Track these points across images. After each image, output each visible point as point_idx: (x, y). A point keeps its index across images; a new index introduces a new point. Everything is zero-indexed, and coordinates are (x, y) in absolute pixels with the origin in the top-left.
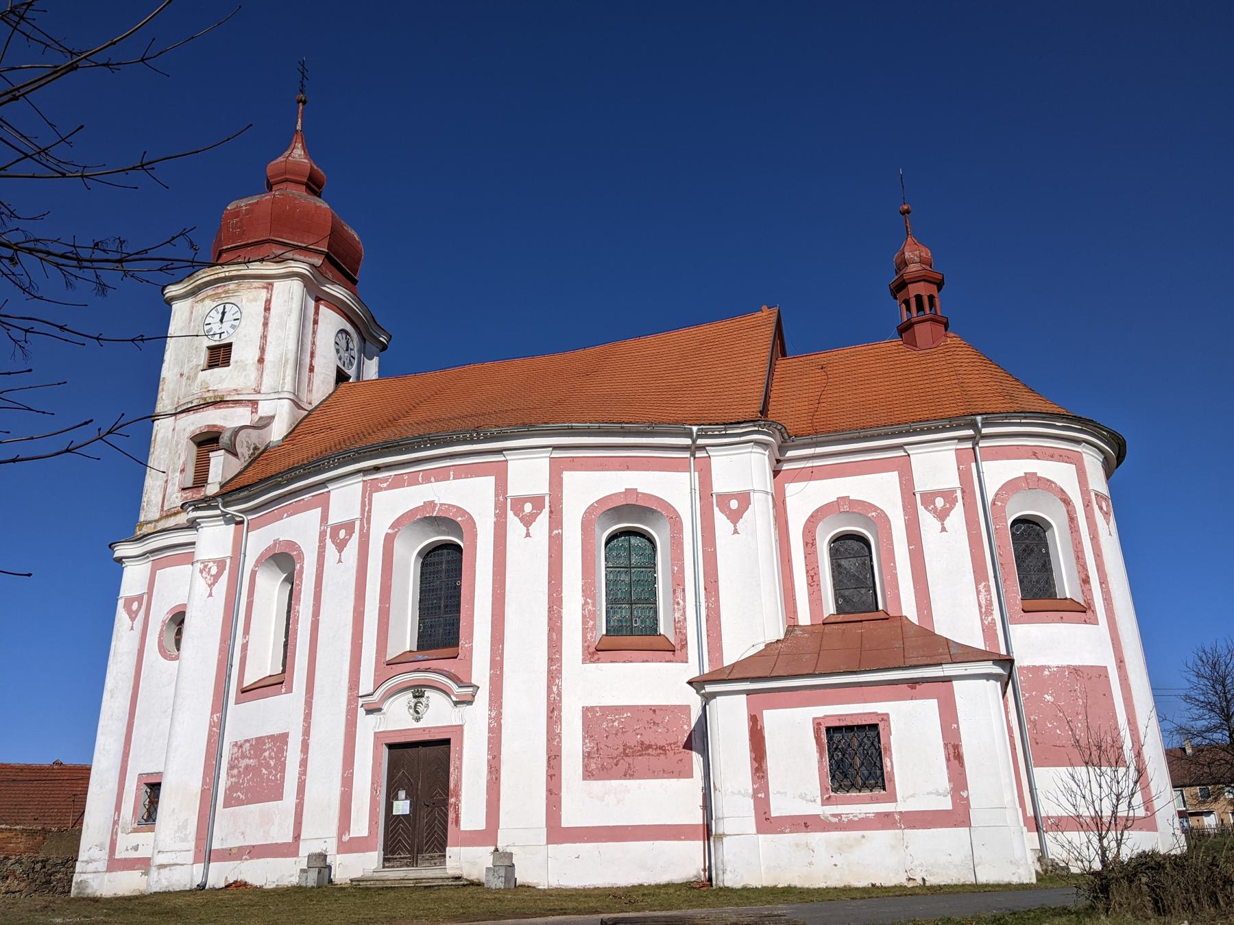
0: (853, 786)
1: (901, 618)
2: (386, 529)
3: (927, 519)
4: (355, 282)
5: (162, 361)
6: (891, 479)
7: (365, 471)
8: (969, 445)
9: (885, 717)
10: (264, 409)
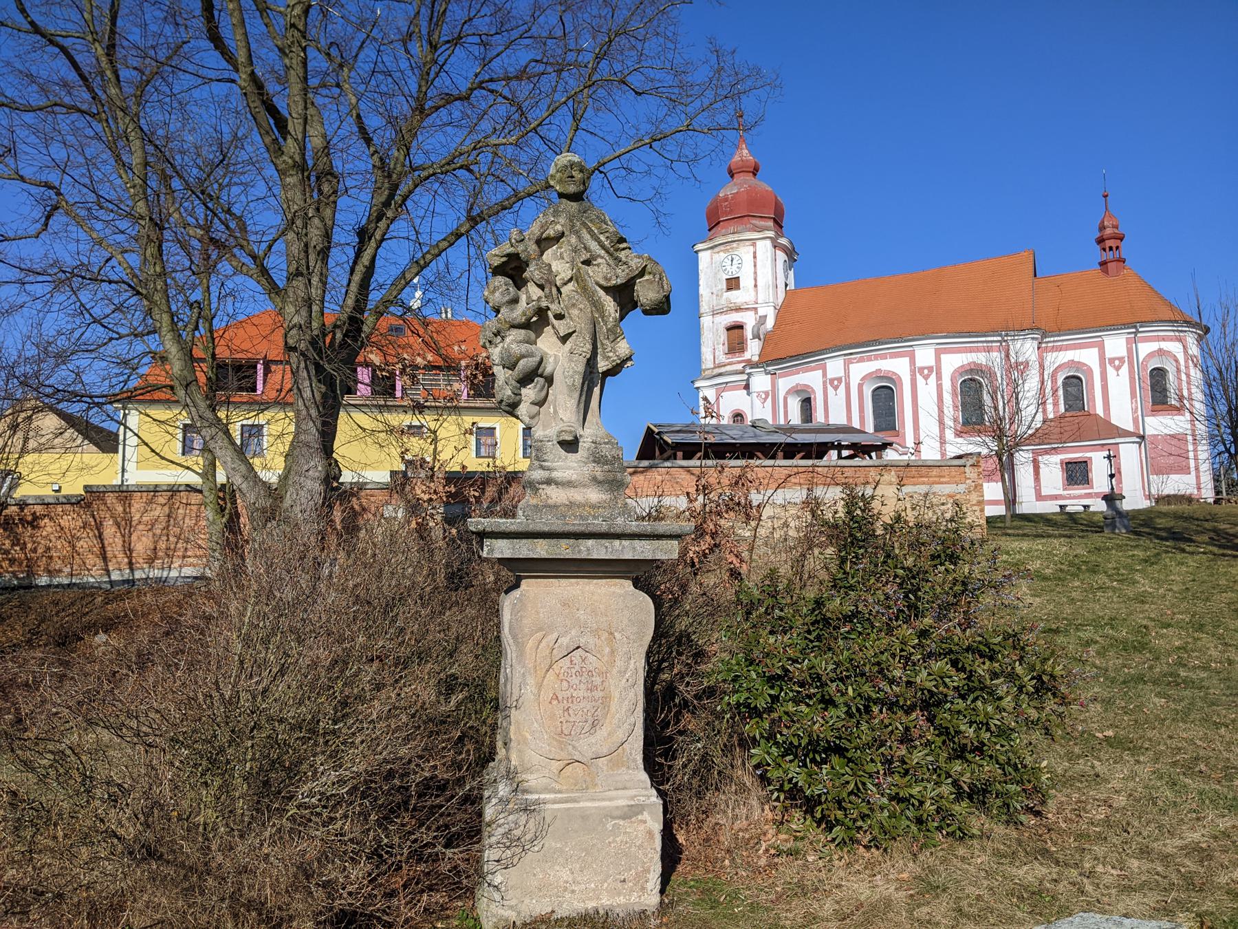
0: (1076, 483)
2: (858, 381)
3: (1110, 371)
4: (781, 227)
5: (698, 285)
6: (1094, 352)
7: (845, 355)
9: (1090, 458)
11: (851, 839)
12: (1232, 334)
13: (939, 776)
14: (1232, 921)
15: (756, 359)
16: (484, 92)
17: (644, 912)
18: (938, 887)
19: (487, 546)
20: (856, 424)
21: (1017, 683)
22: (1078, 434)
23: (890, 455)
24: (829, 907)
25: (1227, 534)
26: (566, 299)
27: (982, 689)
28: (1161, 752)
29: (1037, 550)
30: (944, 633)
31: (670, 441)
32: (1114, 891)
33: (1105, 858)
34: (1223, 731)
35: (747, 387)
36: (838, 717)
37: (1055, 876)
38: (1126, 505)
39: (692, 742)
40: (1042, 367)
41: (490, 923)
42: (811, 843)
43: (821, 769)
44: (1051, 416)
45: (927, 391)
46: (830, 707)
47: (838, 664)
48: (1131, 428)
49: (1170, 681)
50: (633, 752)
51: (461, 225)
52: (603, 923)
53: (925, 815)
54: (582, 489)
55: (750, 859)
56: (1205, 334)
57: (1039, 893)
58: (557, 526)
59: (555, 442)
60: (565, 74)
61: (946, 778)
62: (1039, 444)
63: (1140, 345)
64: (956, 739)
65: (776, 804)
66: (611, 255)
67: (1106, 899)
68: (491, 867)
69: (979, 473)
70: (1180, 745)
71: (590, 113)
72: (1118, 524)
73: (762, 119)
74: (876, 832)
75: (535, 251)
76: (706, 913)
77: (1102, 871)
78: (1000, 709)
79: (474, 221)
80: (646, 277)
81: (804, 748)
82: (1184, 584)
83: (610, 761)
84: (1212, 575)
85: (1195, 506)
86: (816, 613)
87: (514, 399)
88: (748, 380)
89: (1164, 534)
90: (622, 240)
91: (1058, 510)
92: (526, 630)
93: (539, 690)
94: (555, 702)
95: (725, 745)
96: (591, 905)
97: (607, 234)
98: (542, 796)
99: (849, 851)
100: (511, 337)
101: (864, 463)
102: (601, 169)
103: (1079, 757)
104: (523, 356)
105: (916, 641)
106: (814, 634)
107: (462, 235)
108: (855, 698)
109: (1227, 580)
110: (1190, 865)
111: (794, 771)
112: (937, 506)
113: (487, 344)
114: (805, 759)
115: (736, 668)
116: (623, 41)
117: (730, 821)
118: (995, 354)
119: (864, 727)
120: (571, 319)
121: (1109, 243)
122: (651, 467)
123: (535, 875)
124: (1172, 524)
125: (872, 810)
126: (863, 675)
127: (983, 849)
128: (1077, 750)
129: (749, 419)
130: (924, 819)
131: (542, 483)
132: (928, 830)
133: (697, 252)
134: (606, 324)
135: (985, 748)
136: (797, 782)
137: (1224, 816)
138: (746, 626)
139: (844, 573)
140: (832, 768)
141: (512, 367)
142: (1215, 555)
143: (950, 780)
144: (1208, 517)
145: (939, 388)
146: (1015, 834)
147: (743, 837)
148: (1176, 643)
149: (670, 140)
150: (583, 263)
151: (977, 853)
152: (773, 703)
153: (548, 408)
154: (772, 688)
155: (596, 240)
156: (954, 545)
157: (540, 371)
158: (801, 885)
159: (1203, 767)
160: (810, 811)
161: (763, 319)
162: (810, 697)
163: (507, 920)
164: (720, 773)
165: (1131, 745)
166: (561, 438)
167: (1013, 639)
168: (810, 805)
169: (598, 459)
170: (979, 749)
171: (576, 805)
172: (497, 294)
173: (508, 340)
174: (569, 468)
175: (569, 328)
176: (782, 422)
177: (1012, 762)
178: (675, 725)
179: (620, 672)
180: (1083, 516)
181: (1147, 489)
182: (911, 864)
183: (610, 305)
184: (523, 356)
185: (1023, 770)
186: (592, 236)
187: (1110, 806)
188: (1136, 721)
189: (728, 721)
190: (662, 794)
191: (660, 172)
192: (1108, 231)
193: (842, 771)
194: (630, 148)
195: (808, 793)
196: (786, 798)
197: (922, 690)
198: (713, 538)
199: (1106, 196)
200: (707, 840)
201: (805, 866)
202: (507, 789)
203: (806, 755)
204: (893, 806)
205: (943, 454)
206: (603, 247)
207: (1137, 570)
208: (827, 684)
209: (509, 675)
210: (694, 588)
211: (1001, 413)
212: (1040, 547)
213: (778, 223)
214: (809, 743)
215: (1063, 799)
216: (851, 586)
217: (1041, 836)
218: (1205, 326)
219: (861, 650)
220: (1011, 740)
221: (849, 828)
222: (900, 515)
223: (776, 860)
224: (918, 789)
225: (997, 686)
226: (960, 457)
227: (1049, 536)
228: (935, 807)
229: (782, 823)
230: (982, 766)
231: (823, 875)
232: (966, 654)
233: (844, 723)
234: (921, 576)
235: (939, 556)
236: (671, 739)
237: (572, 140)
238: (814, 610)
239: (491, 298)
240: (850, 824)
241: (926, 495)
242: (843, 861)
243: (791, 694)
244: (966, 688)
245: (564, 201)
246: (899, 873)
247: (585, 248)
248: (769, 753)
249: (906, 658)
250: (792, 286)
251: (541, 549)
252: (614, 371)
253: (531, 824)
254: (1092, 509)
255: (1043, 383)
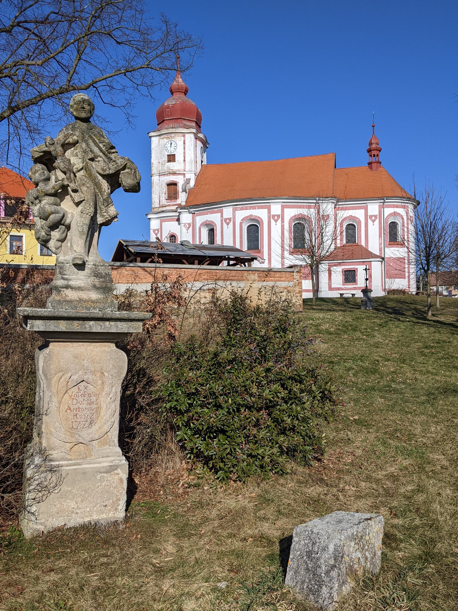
0: (349, 282)
1: (361, 246)
2: (240, 221)
3: (370, 222)
5: (151, 157)
7: (234, 205)
8: (382, 204)
9: (357, 269)
10: (187, 176)
11: (227, 477)
12: (430, 207)
13: (272, 443)
14: (404, 510)
15: (184, 204)
16: (21, 29)
17: (116, 521)
18: (269, 500)
19: (30, 324)
20: (238, 246)
21: (313, 395)
22: (351, 256)
23: (255, 264)
24: (214, 512)
25: (421, 311)
26: (79, 180)
27: (295, 398)
28: (380, 427)
29: (327, 318)
30: (278, 370)
31: (133, 251)
32: (352, 498)
33: (350, 482)
34: (409, 416)
35: (178, 220)
36: (223, 414)
37: (326, 492)
38: (373, 295)
39: (145, 428)
40: (336, 219)
41: (29, 533)
42: (206, 480)
43: (213, 441)
44: (339, 246)
45: (276, 228)
46: (219, 409)
47: (224, 387)
48: (378, 253)
49: (388, 389)
50: (113, 437)
51: (4, 112)
52: (94, 529)
53: (265, 464)
54: (87, 292)
55: (174, 490)
56: (418, 205)
57: (318, 501)
58: (71, 312)
59: (71, 264)
60: (73, 25)
61: (276, 444)
62: (332, 260)
63: (385, 209)
64: (282, 425)
65: (189, 460)
66: (106, 156)
67: (349, 503)
68: (30, 503)
69: (301, 276)
70: (389, 423)
71: (88, 50)
72: (368, 305)
73: (191, 66)
74: (240, 473)
75: (61, 151)
76: (149, 520)
77: (348, 488)
78: (303, 409)
79: (13, 109)
80: (127, 170)
81: (205, 431)
82: (398, 338)
83: (100, 442)
84: (411, 333)
85: (406, 296)
86: (214, 360)
87: (46, 237)
88: (179, 216)
89: (390, 310)
90: (113, 148)
91: (339, 296)
92: (53, 372)
93: (60, 404)
94: (69, 411)
95: (162, 429)
96: (87, 520)
97: (104, 144)
98: (61, 463)
99: (226, 484)
100: (45, 201)
101: (241, 269)
102: (94, 85)
103: (341, 430)
104: (52, 213)
105: (264, 374)
106: (213, 371)
107: (5, 118)
108: (232, 404)
109: (419, 336)
110: (389, 484)
111: (200, 443)
112: (278, 293)
113: (30, 204)
114: (205, 436)
115: (170, 389)
116: (110, 9)
117: (164, 470)
118: (312, 210)
119: (236, 419)
120: (82, 192)
121: (373, 152)
122: (121, 266)
123: (55, 506)
124: (394, 305)
125: (238, 462)
126: (237, 392)
127: (292, 480)
128: (340, 426)
129: (179, 240)
130: (264, 466)
131: (63, 288)
132: (266, 471)
133: (150, 137)
134: (102, 196)
135: (295, 428)
136: (200, 449)
137: (406, 459)
138: (177, 366)
139: (230, 338)
140: (219, 441)
141: (46, 219)
142: (414, 322)
143: (277, 445)
144: (413, 302)
145: (283, 227)
146: (307, 471)
147: (171, 478)
148: (392, 370)
149: (136, 72)
150: (90, 159)
151: (289, 481)
152: (189, 407)
153: (67, 244)
154: (189, 399)
155: (97, 147)
156: (285, 323)
157: (63, 222)
158: (200, 503)
159: (399, 435)
160: (206, 463)
161: (188, 181)
162: (209, 404)
163: (38, 530)
164: (159, 444)
165: (366, 424)
166: (75, 262)
167: (312, 373)
168: (207, 460)
169: (97, 275)
170: (293, 429)
171: (80, 467)
172: (37, 175)
173: (43, 202)
174: (79, 279)
175: (81, 198)
176: (198, 243)
177: (308, 435)
178: (135, 420)
179: (106, 394)
180: (351, 299)
181: (384, 286)
182: (256, 489)
183: (105, 185)
184: (52, 213)
185: (313, 439)
186: (95, 144)
187: (354, 455)
188: (369, 411)
189: (164, 416)
190: (128, 458)
191: (130, 90)
192: (374, 146)
193: (224, 443)
194: (112, 74)
195: (206, 454)
196: (194, 457)
197: (266, 399)
198: (160, 317)
199: (373, 126)
200: (151, 481)
201: (203, 492)
202: (40, 460)
203: (206, 435)
204: (249, 460)
205: (283, 265)
206: (101, 151)
207: (376, 330)
208: (218, 397)
209: (42, 396)
210: (149, 344)
211: (314, 243)
212: (329, 316)
213: (198, 125)
214: (208, 428)
215: (332, 452)
216: (233, 344)
217: (320, 472)
218: (417, 201)
219: (236, 378)
220: (309, 423)
221: (226, 472)
222: (259, 307)
223: (188, 490)
224: (262, 450)
225: (303, 397)
226: (291, 267)
227: (334, 311)
228: (270, 459)
229: (191, 470)
230: (293, 437)
231: (212, 497)
232: (288, 381)
233: (226, 417)
234: (268, 341)
235: (277, 328)
236: (134, 428)
237: (76, 65)
238: (213, 358)
239: (33, 177)
240: (227, 470)
241: (273, 287)
242: (222, 488)
243: (199, 402)
244: (288, 398)
245: (78, 121)
246: (251, 493)
247: (91, 151)
248: (186, 434)
249: (259, 382)
250: (205, 163)
251: (62, 326)
252: (107, 223)
253: (54, 479)
254: (356, 296)
255: (335, 228)
